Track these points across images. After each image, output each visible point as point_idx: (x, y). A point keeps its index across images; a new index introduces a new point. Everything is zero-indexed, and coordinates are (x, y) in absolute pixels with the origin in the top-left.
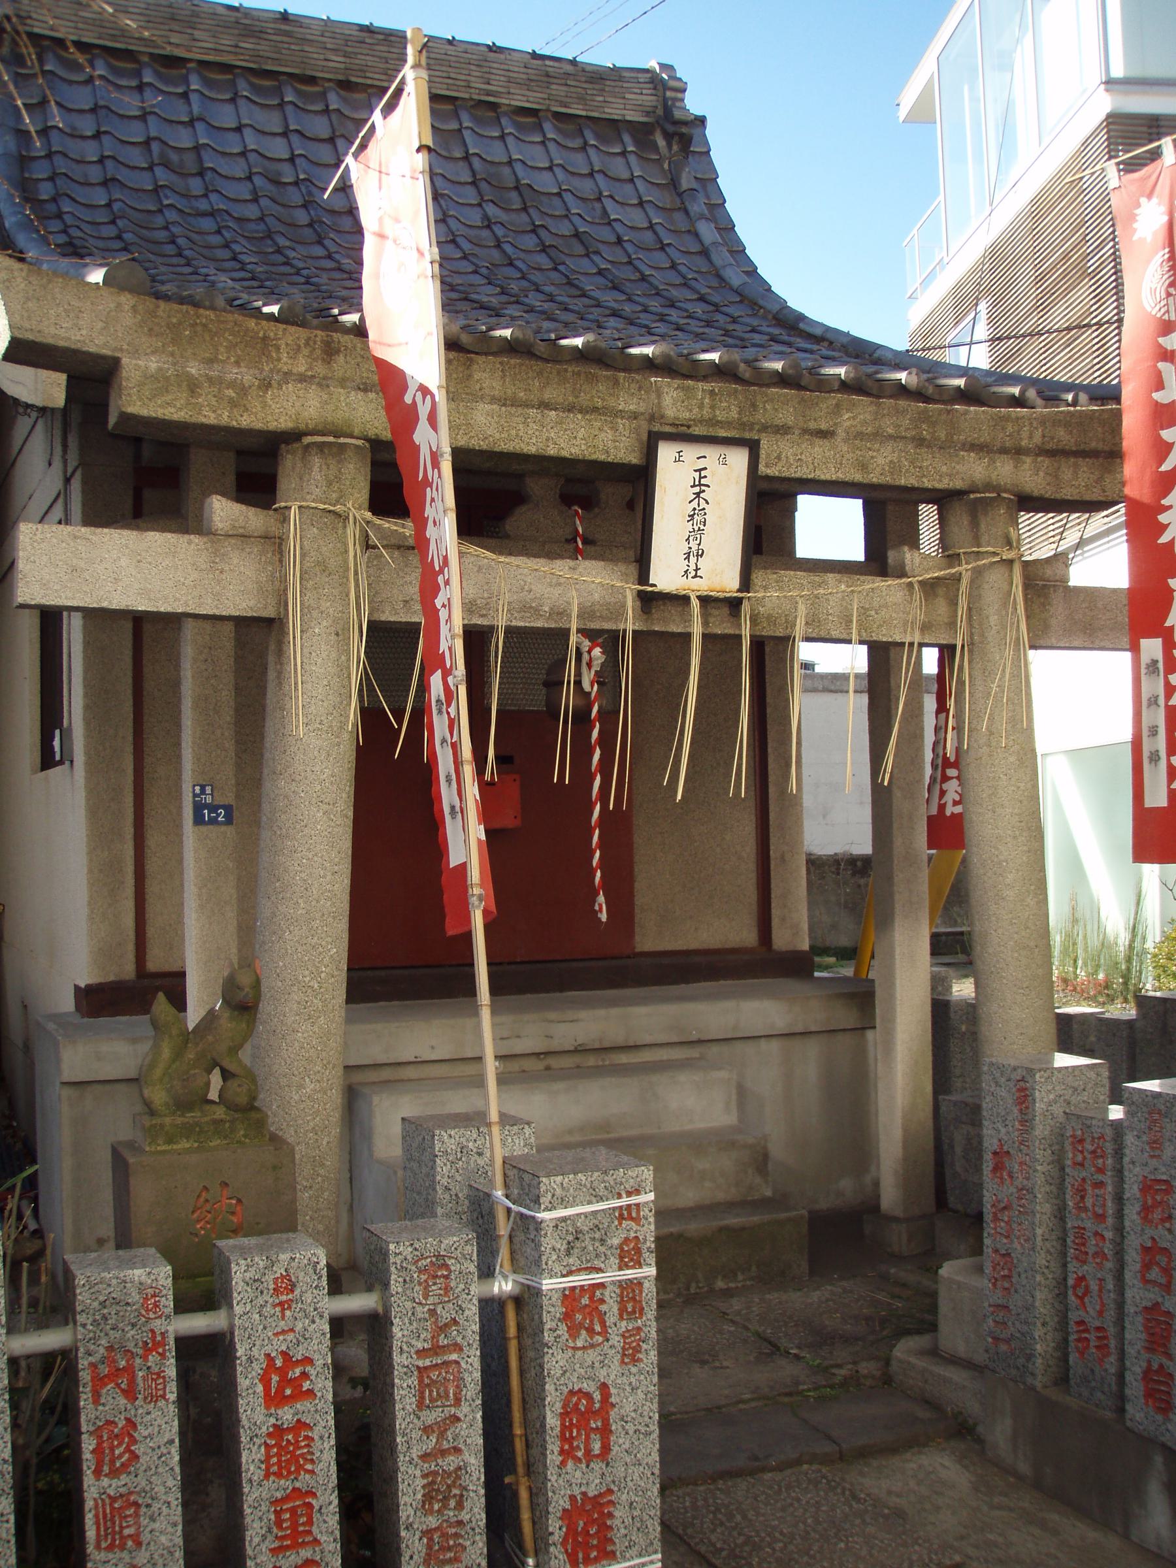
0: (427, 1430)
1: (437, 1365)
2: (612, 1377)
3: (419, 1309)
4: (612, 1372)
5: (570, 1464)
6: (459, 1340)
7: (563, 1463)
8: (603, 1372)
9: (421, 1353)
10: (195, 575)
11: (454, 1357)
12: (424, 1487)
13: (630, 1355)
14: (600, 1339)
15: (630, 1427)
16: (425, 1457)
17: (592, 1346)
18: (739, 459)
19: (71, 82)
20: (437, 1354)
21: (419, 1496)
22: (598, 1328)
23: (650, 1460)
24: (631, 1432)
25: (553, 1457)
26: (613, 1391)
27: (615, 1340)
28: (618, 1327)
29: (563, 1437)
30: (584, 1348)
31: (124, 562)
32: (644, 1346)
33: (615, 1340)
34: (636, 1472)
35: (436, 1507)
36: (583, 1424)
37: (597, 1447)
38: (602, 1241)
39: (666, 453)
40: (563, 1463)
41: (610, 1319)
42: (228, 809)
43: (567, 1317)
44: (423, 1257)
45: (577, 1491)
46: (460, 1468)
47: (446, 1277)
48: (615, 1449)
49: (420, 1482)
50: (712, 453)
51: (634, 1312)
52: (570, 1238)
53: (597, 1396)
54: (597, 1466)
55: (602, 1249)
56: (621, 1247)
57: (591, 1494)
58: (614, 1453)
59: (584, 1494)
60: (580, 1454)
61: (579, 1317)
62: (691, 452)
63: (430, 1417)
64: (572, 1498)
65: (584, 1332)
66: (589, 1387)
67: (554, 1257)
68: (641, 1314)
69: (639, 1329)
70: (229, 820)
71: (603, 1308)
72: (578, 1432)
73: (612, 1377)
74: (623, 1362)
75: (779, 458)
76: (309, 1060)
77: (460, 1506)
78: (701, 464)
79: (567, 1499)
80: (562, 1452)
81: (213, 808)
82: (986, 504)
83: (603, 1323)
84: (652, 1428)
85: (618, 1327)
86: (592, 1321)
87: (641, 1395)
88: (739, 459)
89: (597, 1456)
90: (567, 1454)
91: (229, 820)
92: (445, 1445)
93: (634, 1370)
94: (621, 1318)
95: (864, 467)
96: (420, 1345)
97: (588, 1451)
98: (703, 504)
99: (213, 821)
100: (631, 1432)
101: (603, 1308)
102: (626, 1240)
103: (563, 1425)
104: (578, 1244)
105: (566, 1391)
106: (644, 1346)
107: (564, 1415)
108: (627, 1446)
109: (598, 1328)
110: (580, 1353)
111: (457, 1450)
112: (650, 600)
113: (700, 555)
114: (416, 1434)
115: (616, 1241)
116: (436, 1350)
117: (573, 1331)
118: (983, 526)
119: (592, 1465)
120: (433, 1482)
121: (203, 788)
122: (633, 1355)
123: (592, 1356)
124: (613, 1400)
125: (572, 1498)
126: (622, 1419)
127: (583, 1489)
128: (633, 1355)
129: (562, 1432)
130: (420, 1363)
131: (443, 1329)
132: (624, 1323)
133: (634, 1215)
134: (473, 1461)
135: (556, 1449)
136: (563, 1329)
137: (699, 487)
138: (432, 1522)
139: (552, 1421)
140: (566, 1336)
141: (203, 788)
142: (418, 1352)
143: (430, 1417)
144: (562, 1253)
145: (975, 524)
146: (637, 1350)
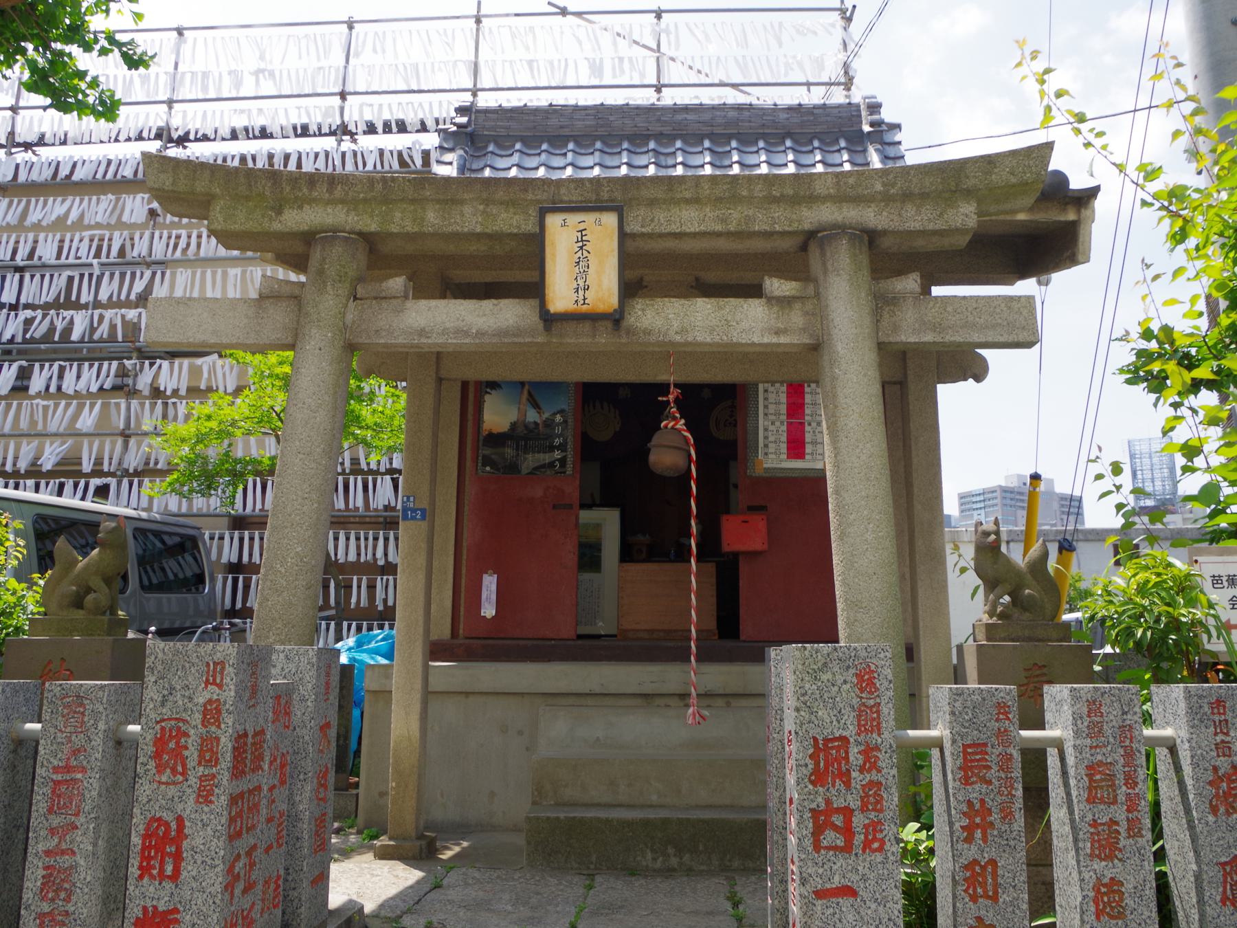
0: (53, 831)
1: (66, 781)
2: (188, 812)
3: (59, 735)
4: (188, 807)
5: (146, 879)
6: (85, 763)
7: (141, 877)
8: (181, 806)
9: (56, 770)
10: (246, 321)
11: (79, 776)
12: (44, 877)
13: (205, 796)
14: (180, 778)
15: (198, 858)
16: (48, 853)
17: (174, 783)
18: (610, 220)
19: (502, 156)
20: (68, 772)
21: (39, 884)
22: (180, 769)
23: (212, 889)
24: (199, 862)
25: (134, 871)
26: (187, 824)
27: (193, 781)
28: (197, 771)
29: (143, 858)
30: (167, 784)
31: (205, 315)
32: (217, 791)
33: (193, 781)
34: (200, 898)
35: (50, 895)
36: (160, 849)
37: (169, 869)
38: (190, 699)
39: (553, 221)
40: (141, 877)
41: (191, 763)
42: (423, 511)
43: (157, 755)
44: (67, 696)
45: (149, 904)
46: (71, 867)
47: (83, 714)
48: (184, 874)
49: (41, 872)
50: (590, 218)
51: (210, 761)
52: (166, 692)
53: (174, 826)
54: (168, 885)
55: (190, 705)
56: (205, 705)
57: (160, 909)
58: (182, 877)
59: (155, 907)
60: (155, 872)
61: (166, 757)
62: (574, 219)
63: (56, 821)
64: (145, 909)
65: (168, 770)
66: (168, 816)
67: (151, 706)
68: (215, 766)
69: (214, 776)
70: (423, 518)
71: (186, 753)
72: (156, 853)
73: (188, 812)
74: (197, 802)
75: (652, 220)
76: (273, 620)
77: (68, 900)
78: (582, 226)
79: (140, 908)
80: (141, 868)
81: (414, 511)
82: (830, 238)
83: (184, 766)
84: (217, 862)
85: (197, 771)
86: (176, 763)
87: (210, 832)
88: (610, 220)
89: (168, 877)
90: (145, 870)
91: (423, 518)
92: (64, 846)
93: (206, 809)
94: (200, 764)
95: (724, 221)
96: (56, 763)
97: (162, 870)
98: (585, 254)
99: (413, 518)
100: (199, 862)
101: (186, 753)
102: (210, 701)
103: (143, 844)
104: (171, 698)
105: (149, 816)
106: (217, 791)
107: (146, 836)
108: (194, 873)
109: (180, 769)
110: (163, 787)
111: (74, 853)
112: (550, 320)
113: (586, 288)
114: (43, 833)
115: (201, 700)
116: (68, 769)
117: (160, 769)
118: (828, 254)
119: (164, 884)
120: (51, 875)
121: (408, 498)
122: (207, 796)
123: (172, 791)
124: (186, 831)
125: (145, 909)
126: (192, 849)
127: (155, 903)
128: (207, 796)
129: (143, 850)
130: (54, 777)
131: (75, 752)
132: (201, 769)
133: (218, 681)
134: (82, 862)
135: (136, 864)
136: (152, 765)
137: (582, 243)
138: (46, 907)
139: (136, 840)
140: (154, 771)
141: (408, 498)
142: (54, 768)
143: (56, 821)
144: (158, 704)
145: (823, 254)
146: (210, 793)
